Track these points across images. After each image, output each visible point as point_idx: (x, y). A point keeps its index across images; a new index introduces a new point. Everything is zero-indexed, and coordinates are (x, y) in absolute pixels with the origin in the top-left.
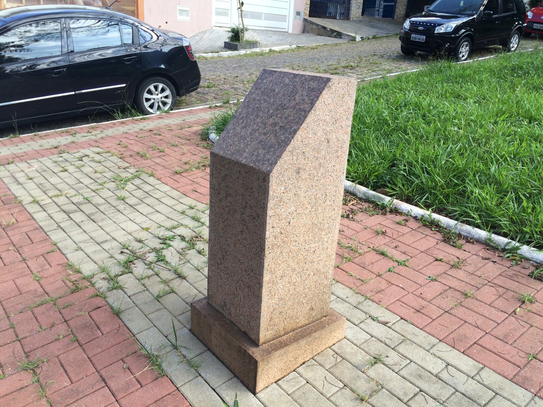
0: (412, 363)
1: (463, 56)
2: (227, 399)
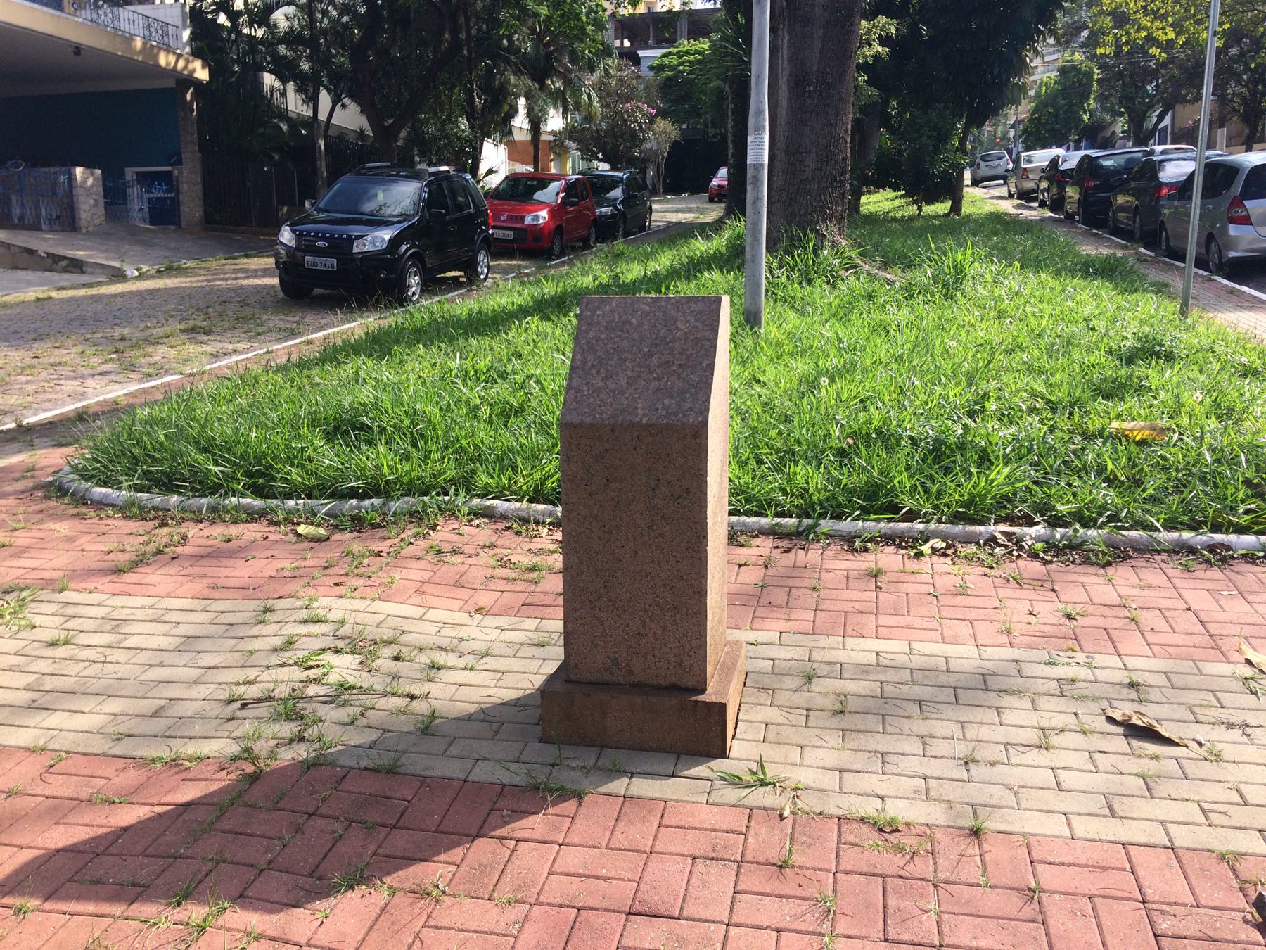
0: (771, 727)
1: (414, 294)
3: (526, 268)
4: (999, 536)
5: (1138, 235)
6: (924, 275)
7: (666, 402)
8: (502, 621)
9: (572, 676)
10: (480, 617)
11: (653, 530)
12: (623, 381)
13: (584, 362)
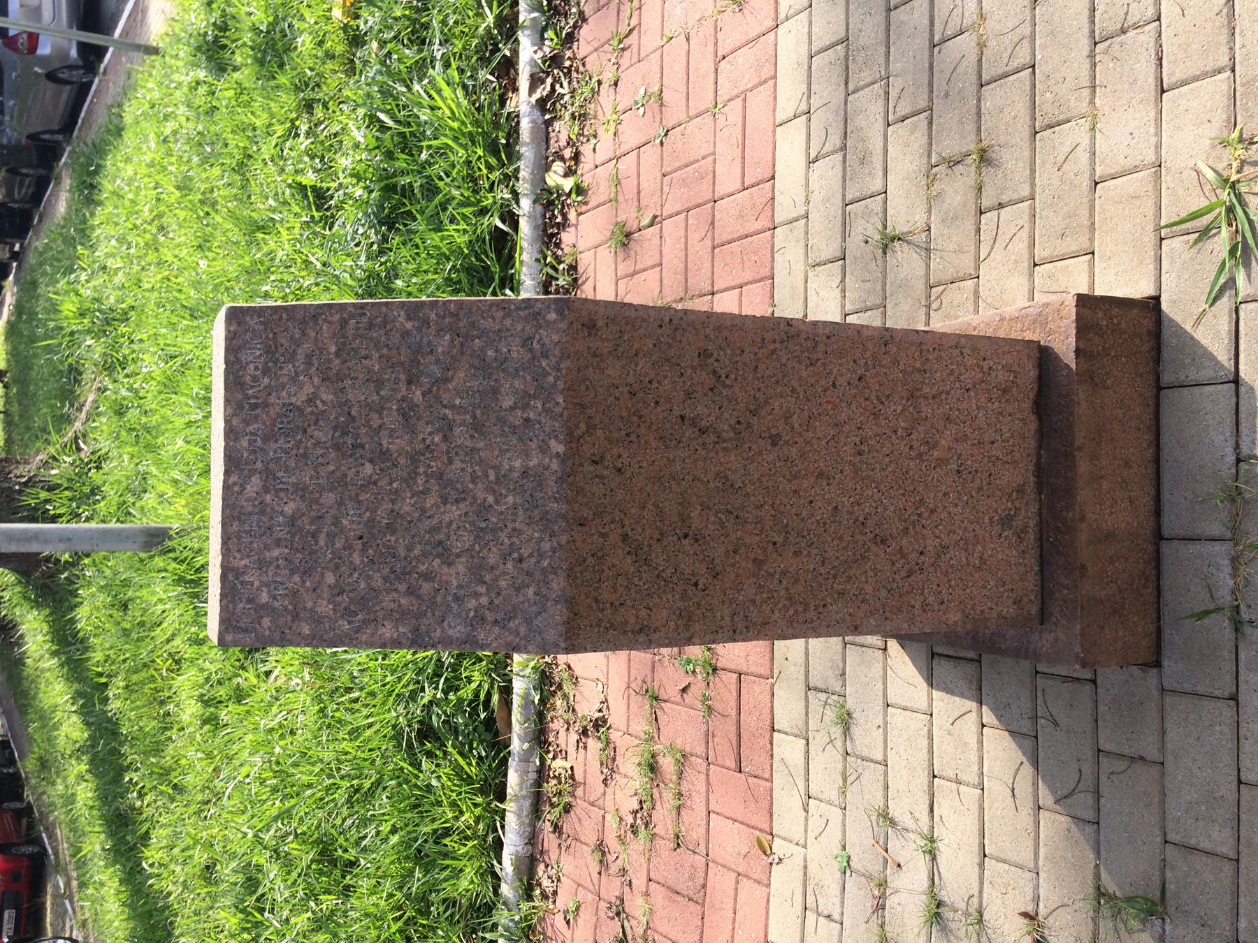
2: (1225, 325)
3: (57, 886)
4: (537, 95)
5: (42, 172)
6: (93, 349)
7: (508, 402)
8: (787, 801)
9: (1034, 610)
10: (778, 845)
11: (779, 436)
12: (454, 512)
13: (401, 615)
